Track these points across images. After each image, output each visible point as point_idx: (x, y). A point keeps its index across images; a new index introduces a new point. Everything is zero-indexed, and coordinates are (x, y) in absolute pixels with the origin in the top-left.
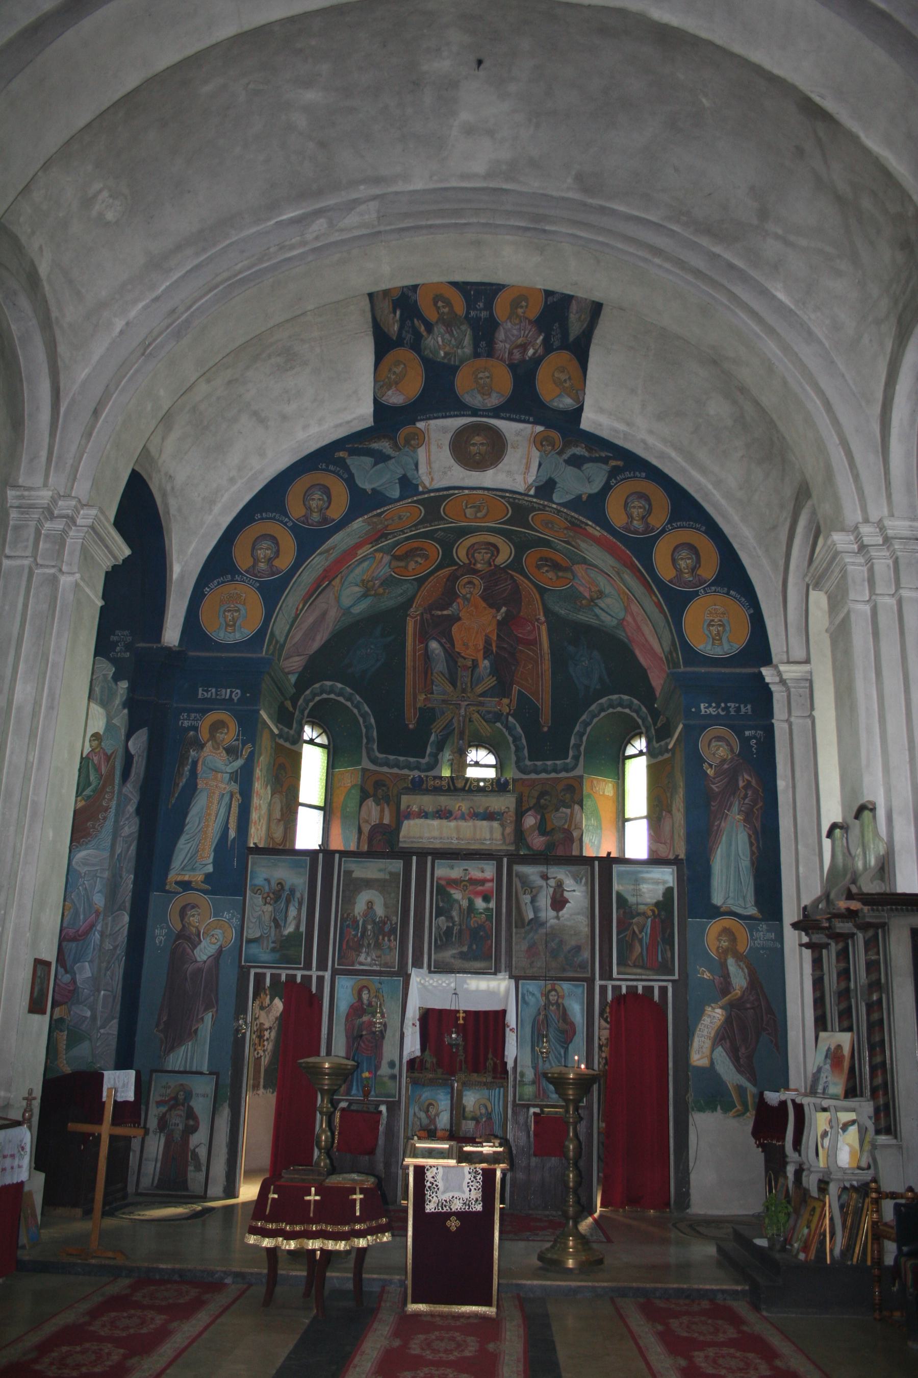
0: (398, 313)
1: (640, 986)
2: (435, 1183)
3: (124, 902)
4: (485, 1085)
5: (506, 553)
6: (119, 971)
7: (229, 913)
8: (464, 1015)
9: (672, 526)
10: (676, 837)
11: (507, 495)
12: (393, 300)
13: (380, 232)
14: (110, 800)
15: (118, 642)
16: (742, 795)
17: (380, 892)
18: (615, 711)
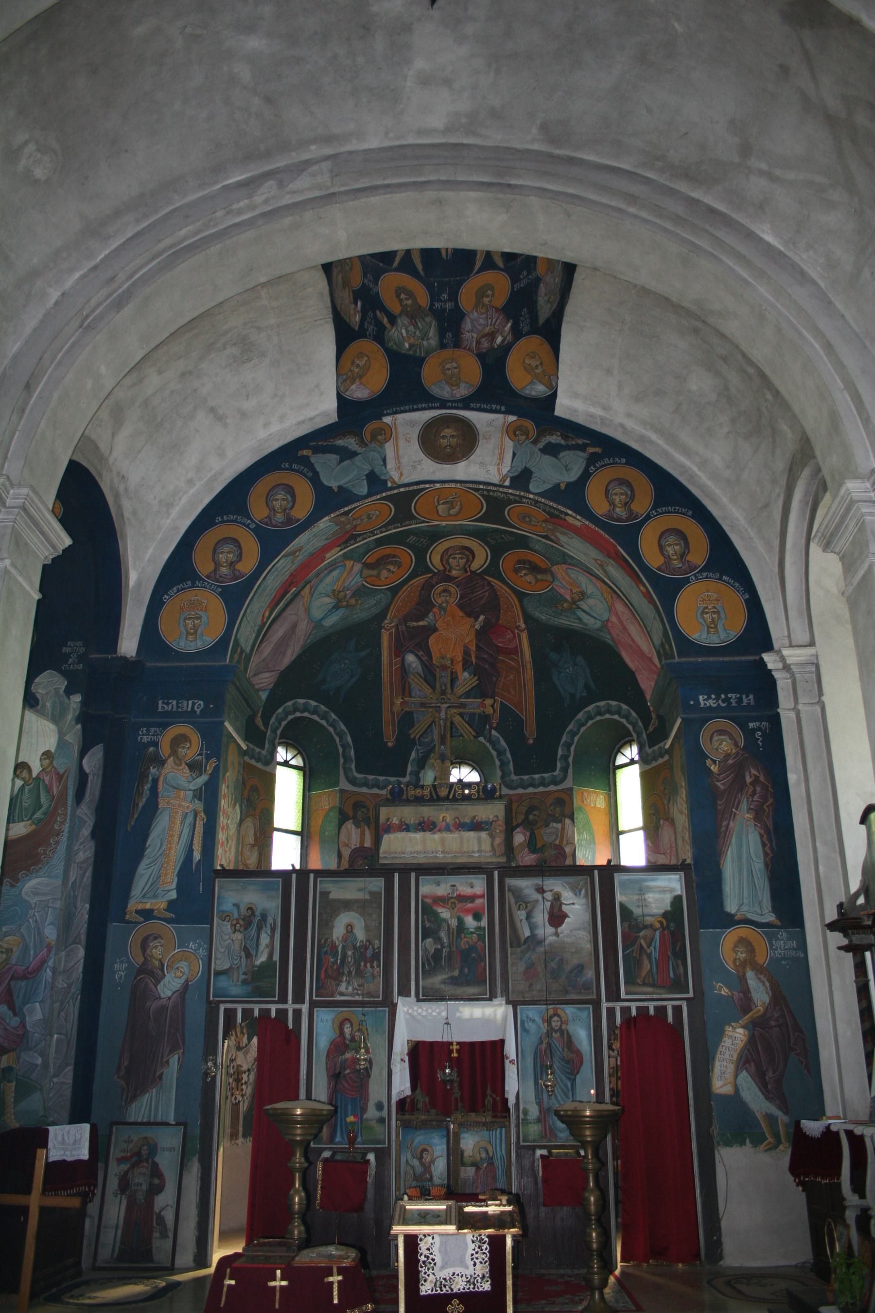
0: (359, 304)
1: (651, 1006)
2: (431, 1256)
3: (79, 934)
4: (484, 1125)
5: (482, 558)
6: (73, 1010)
7: (195, 943)
8: (458, 1047)
9: (656, 511)
10: (680, 842)
11: (481, 487)
12: (353, 290)
13: (334, 194)
14: (63, 823)
15: (70, 653)
16: (750, 791)
17: (361, 914)
18: (603, 718)
